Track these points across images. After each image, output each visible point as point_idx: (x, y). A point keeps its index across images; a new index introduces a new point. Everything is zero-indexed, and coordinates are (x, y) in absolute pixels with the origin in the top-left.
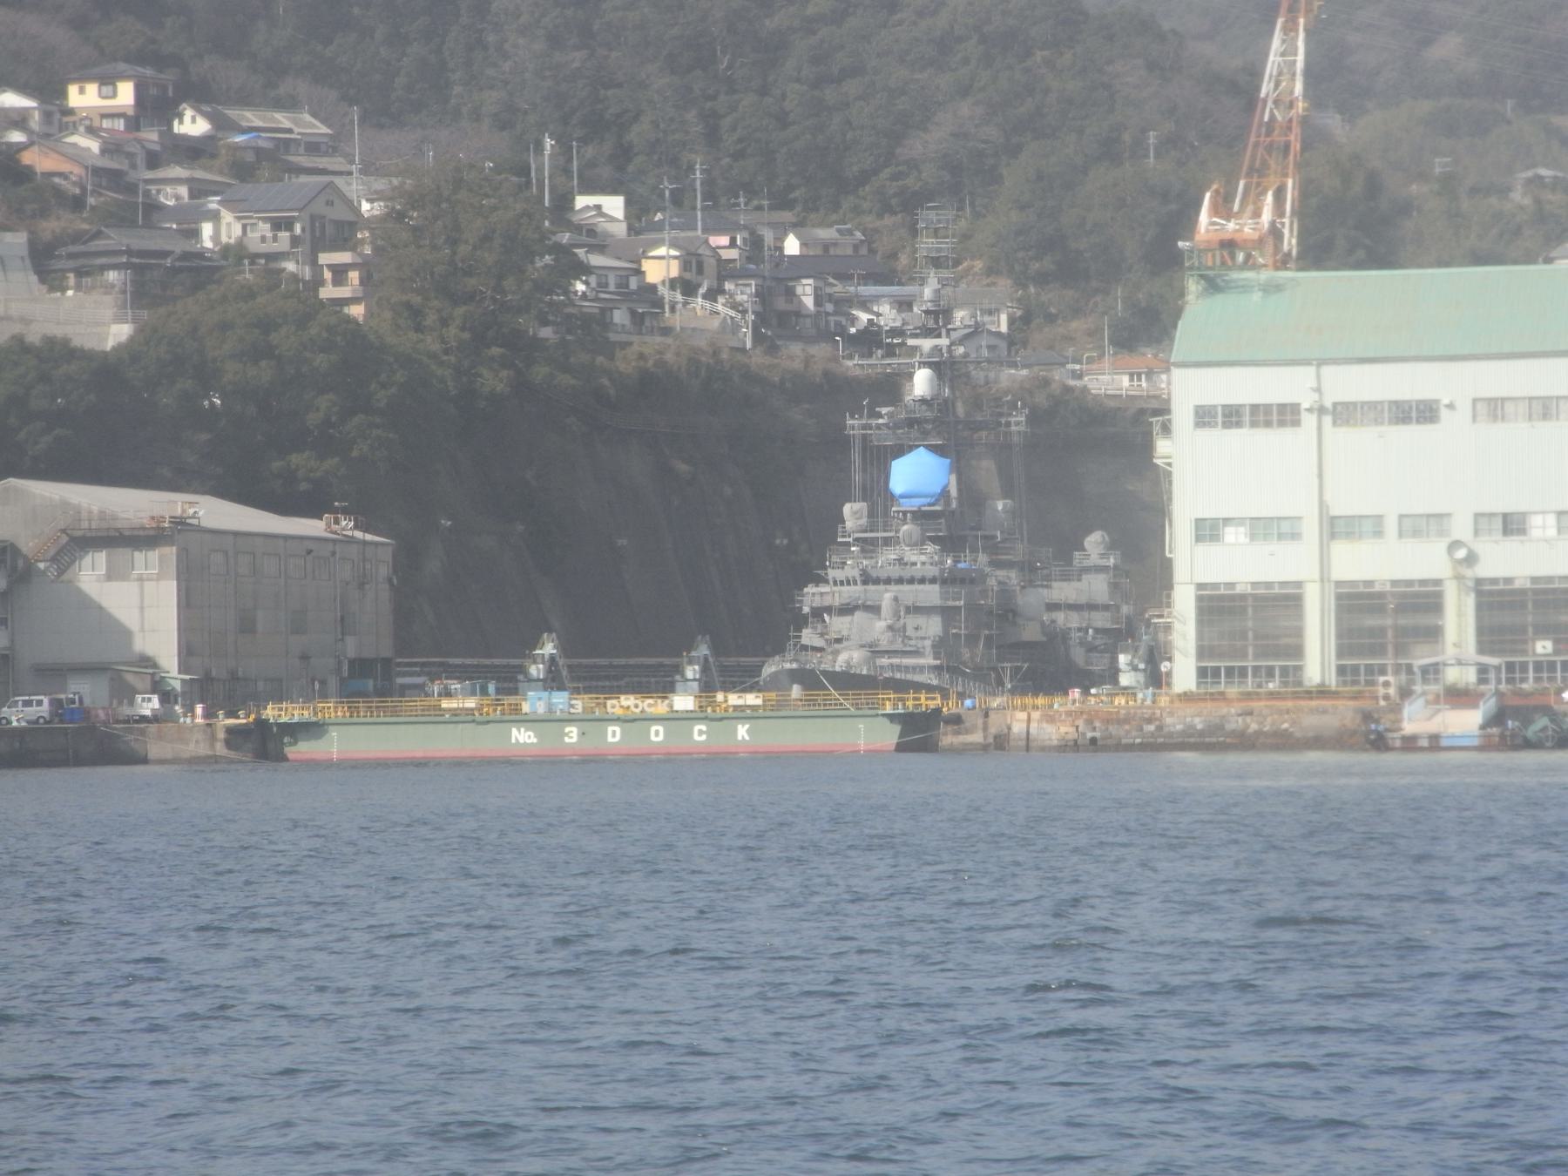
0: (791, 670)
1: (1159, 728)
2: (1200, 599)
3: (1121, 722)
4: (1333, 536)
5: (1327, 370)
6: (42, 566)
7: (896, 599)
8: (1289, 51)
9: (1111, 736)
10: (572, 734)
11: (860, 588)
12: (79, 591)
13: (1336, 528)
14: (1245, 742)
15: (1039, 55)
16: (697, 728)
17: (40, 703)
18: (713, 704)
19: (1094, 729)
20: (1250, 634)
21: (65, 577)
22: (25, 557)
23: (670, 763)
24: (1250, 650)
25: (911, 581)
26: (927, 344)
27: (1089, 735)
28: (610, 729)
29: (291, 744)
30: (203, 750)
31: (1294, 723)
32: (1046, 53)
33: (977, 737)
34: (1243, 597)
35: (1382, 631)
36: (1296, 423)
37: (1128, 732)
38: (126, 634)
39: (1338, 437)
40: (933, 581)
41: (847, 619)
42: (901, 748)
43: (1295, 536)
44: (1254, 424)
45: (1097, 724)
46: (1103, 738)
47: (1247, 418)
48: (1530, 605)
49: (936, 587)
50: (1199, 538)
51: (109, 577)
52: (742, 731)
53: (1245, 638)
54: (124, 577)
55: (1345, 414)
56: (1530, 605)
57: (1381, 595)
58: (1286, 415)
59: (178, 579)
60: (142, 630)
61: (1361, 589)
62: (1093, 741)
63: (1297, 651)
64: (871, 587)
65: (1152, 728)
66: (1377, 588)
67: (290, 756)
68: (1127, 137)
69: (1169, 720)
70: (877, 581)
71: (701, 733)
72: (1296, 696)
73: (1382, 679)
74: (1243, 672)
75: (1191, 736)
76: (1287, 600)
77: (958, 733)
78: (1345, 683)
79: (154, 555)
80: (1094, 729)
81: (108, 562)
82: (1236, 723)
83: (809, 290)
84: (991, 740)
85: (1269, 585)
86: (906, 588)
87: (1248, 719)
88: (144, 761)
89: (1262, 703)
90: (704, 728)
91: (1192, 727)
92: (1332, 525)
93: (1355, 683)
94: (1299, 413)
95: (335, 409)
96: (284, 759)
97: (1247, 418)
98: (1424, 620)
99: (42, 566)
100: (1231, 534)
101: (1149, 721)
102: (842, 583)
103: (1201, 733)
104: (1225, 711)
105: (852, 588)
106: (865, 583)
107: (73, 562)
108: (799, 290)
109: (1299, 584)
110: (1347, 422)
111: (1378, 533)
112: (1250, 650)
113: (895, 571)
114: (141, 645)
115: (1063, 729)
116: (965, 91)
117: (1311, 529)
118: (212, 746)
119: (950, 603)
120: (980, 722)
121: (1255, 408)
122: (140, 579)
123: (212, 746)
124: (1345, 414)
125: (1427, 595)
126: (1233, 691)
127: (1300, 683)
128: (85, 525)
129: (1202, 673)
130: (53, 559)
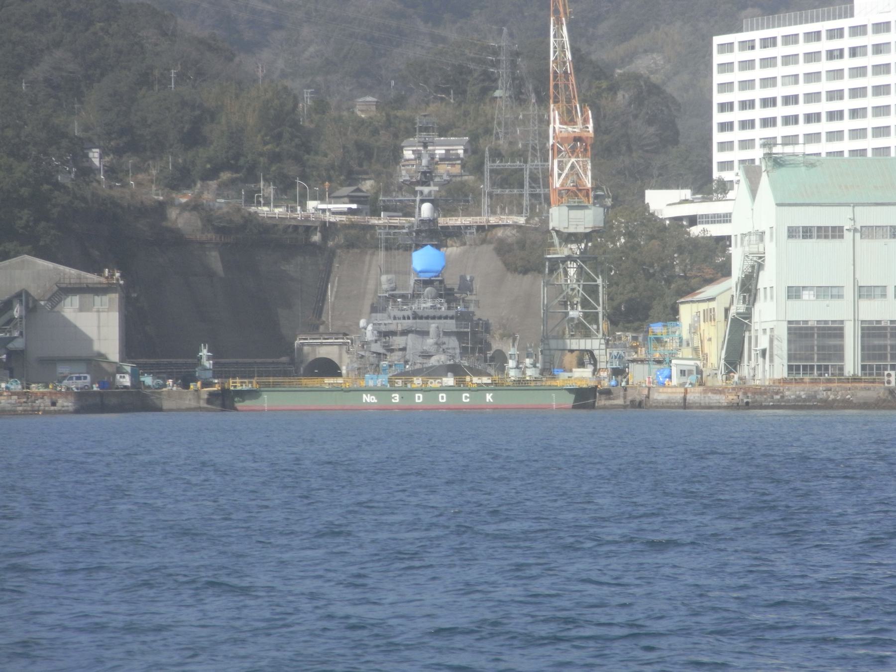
0: (450, 365)
1: (782, 397)
2: (789, 329)
3: (762, 393)
4: (860, 296)
5: (857, 208)
6: (42, 303)
7: (438, 327)
8: (558, 35)
9: (756, 401)
10: (396, 398)
11: (411, 321)
12: (63, 316)
13: (864, 292)
14: (827, 405)
15: (99, 25)
16: (464, 395)
17: (85, 378)
18: (464, 382)
19: (748, 397)
20: (816, 348)
21: (56, 309)
22: (33, 298)
23: (432, 412)
24: (816, 357)
25: (440, 318)
26: (426, 190)
27: (745, 400)
28: (417, 395)
29: (240, 402)
30: (193, 404)
31: (853, 395)
32: (102, 24)
33: (620, 401)
34: (812, 328)
35: (885, 347)
36: (841, 237)
37: (766, 399)
38: (90, 341)
39: (864, 245)
40: (452, 318)
41: (404, 338)
42: (574, 407)
43: (840, 297)
44: (819, 237)
45: (750, 395)
46: (753, 402)
47: (815, 234)
48: (816, 335)
49: (454, 321)
50: (789, 297)
51: (81, 309)
52: (489, 397)
53: (813, 350)
54: (89, 310)
55: (868, 232)
56: (816, 335)
57: (885, 328)
58: (836, 232)
59: (120, 311)
60: (99, 339)
61: (830, 325)
62: (747, 403)
63: (841, 358)
64: (418, 321)
65: (778, 397)
66: (883, 324)
67: (239, 408)
68: (156, 73)
69: (787, 393)
70: (421, 318)
71: (466, 397)
72: (840, 381)
73: (886, 373)
74: (812, 367)
75: (799, 401)
76: (834, 331)
77: (610, 399)
78: (865, 374)
79: (106, 298)
80: (748, 397)
81: (80, 301)
82: (822, 395)
83: (97, 155)
84: (628, 403)
85: (826, 322)
86: (443, 321)
87: (829, 393)
88: (160, 409)
89: (836, 385)
90: (468, 395)
91: (799, 396)
92: (860, 291)
93: (871, 374)
94: (843, 231)
95: (32, 218)
96: (236, 409)
97: (815, 234)
98: (832, 342)
99: (42, 303)
100: (806, 295)
101: (777, 393)
102: (399, 319)
103: (805, 400)
104: (817, 388)
105: (407, 321)
106: (414, 318)
107: (60, 301)
108: (91, 155)
109: (842, 322)
110: (868, 237)
111: (884, 296)
112: (816, 357)
113: (432, 313)
114: (97, 347)
115: (730, 397)
116: (58, 44)
117: (849, 293)
118: (198, 402)
119: (462, 330)
120: (622, 393)
121: (819, 228)
122: (98, 311)
123: (198, 402)
124: (868, 232)
125: (835, 329)
126: (807, 378)
127: (842, 375)
128: (67, 281)
129: (790, 368)
130: (49, 300)
